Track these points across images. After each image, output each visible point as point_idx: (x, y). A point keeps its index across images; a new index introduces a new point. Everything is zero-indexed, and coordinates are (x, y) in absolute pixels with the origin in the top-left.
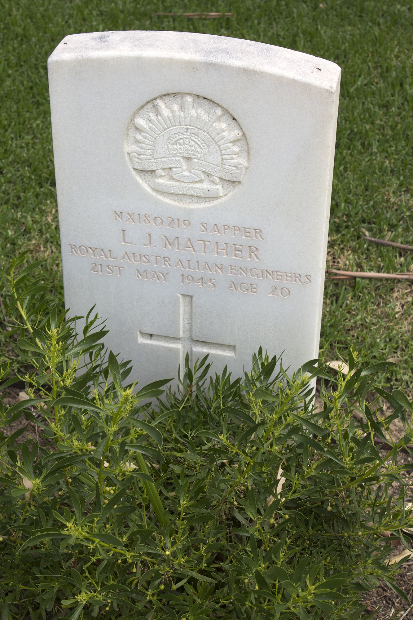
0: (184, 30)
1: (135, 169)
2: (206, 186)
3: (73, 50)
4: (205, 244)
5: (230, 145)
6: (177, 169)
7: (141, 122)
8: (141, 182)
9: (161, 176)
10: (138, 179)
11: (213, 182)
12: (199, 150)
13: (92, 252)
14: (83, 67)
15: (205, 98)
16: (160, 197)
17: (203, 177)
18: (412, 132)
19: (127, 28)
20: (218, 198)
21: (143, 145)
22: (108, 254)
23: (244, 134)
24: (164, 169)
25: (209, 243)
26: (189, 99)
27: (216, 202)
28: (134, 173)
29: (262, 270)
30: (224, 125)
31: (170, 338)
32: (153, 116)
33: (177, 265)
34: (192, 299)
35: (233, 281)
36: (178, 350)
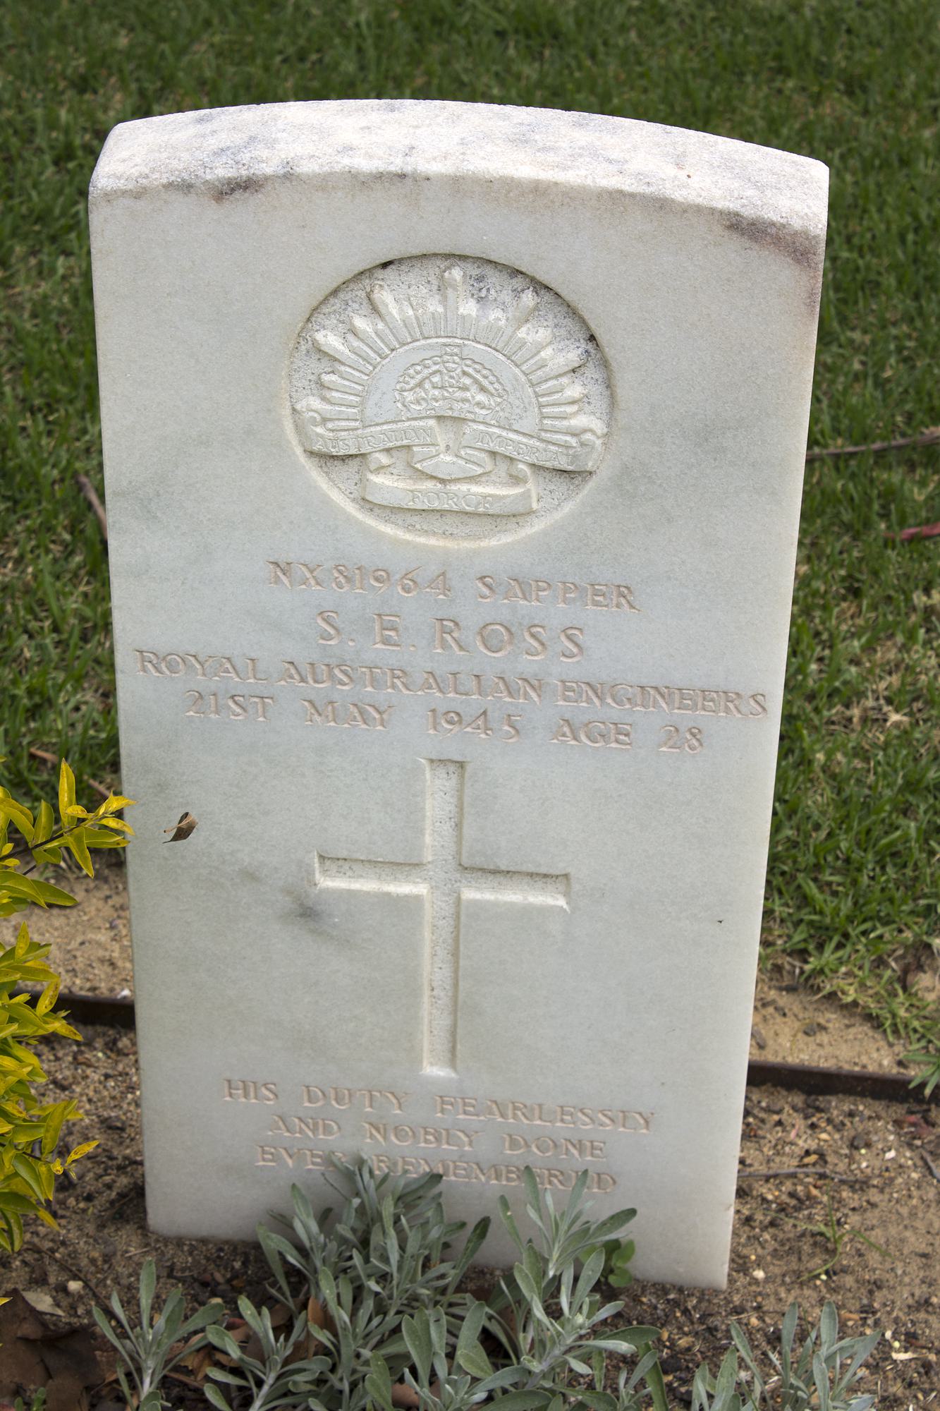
0: (721, 130)
1: (312, 454)
2: (497, 491)
5: (565, 380)
7: (330, 339)
8: (334, 491)
10: (316, 475)
11: (516, 480)
12: (481, 397)
15: (385, 265)
16: (370, 521)
17: (488, 464)
19: (156, 108)
28: (302, 459)
30: (543, 334)
31: (495, 872)
35: (312, 697)
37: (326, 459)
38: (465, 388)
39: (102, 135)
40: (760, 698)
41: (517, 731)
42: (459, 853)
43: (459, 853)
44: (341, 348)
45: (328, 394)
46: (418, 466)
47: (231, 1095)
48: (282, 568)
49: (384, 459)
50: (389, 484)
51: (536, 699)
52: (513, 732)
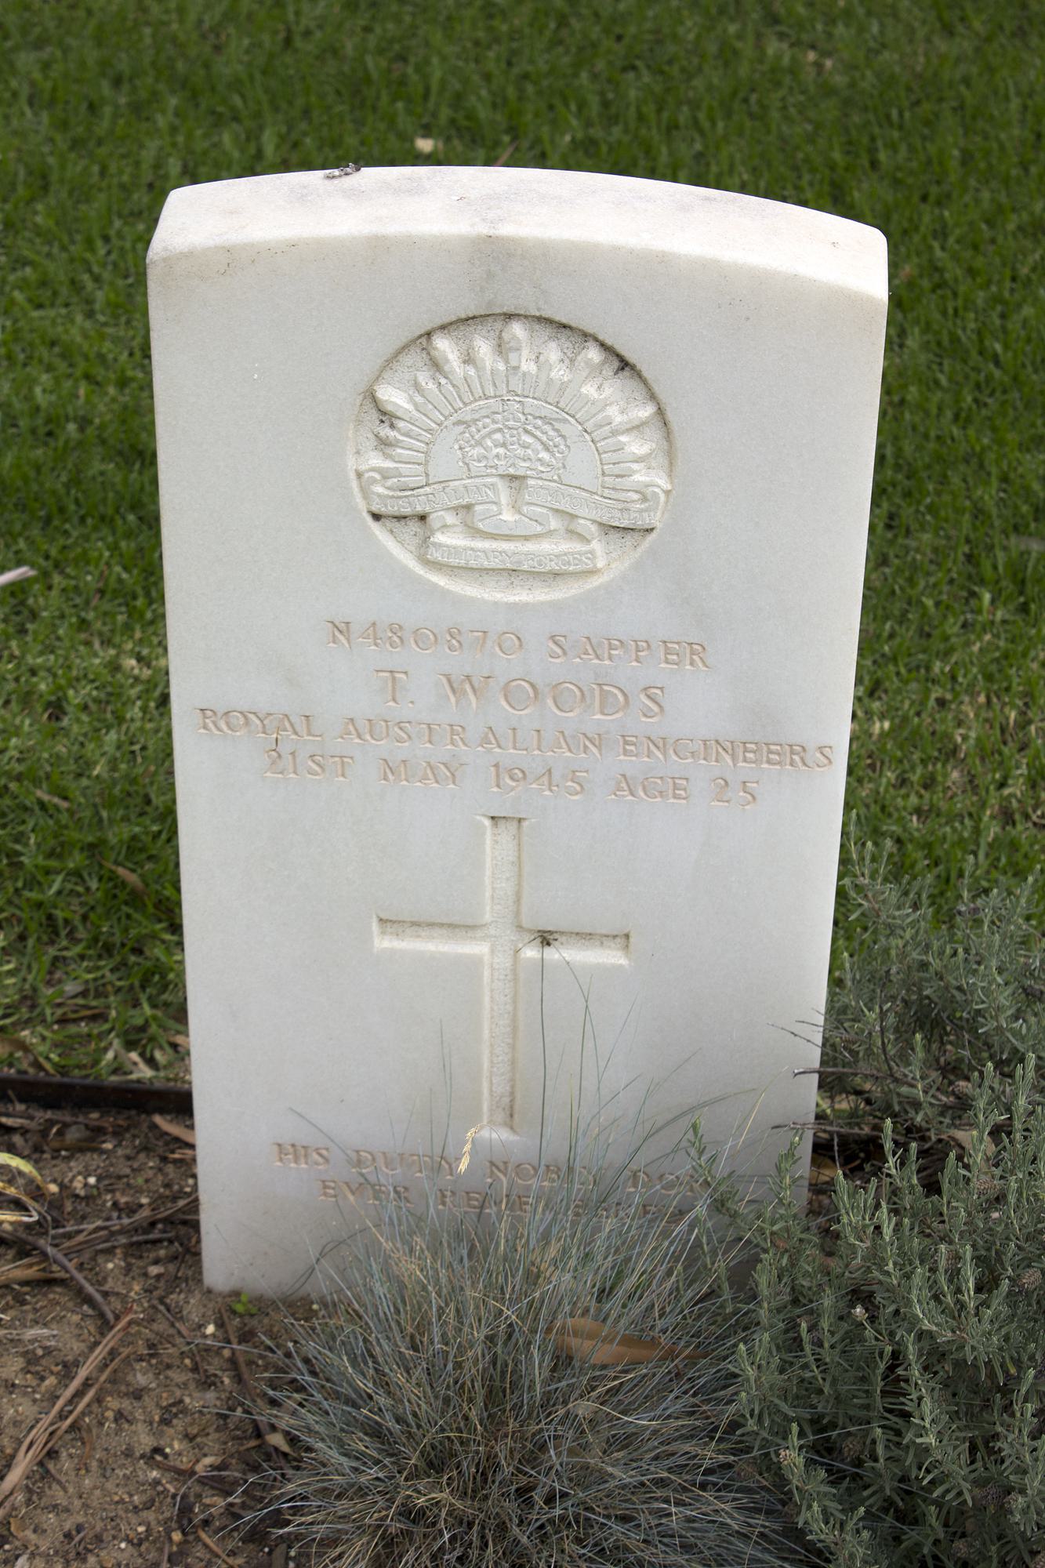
1: (377, 517)
2: (553, 548)
3: (200, 218)
4: (394, 679)
6: (486, 506)
7: (392, 395)
9: (445, 527)
11: (573, 534)
13: (258, 722)
14: (228, 262)
15: (565, 327)
16: (440, 580)
18: (1043, 375)
20: (593, 572)
21: (399, 451)
22: (301, 727)
23: (660, 412)
24: (455, 509)
25: (403, 676)
26: (594, 354)
27: (595, 582)
29: (705, 741)
32: (424, 378)
33: (485, 741)
34: (519, 828)
36: (475, 962)
37: (377, 517)
38: (525, 446)
39: (163, 195)
40: (827, 751)
41: (754, 798)
42: (518, 914)
43: (518, 914)
44: (407, 406)
45: (389, 451)
46: (481, 526)
47: (281, 1160)
48: (340, 629)
49: (450, 518)
50: (450, 539)
51: (729, 761)
52: (578, 788)
